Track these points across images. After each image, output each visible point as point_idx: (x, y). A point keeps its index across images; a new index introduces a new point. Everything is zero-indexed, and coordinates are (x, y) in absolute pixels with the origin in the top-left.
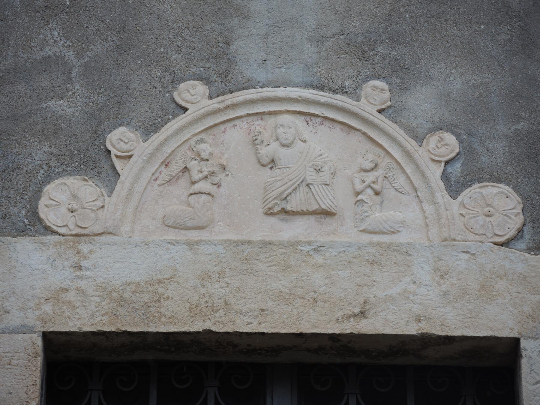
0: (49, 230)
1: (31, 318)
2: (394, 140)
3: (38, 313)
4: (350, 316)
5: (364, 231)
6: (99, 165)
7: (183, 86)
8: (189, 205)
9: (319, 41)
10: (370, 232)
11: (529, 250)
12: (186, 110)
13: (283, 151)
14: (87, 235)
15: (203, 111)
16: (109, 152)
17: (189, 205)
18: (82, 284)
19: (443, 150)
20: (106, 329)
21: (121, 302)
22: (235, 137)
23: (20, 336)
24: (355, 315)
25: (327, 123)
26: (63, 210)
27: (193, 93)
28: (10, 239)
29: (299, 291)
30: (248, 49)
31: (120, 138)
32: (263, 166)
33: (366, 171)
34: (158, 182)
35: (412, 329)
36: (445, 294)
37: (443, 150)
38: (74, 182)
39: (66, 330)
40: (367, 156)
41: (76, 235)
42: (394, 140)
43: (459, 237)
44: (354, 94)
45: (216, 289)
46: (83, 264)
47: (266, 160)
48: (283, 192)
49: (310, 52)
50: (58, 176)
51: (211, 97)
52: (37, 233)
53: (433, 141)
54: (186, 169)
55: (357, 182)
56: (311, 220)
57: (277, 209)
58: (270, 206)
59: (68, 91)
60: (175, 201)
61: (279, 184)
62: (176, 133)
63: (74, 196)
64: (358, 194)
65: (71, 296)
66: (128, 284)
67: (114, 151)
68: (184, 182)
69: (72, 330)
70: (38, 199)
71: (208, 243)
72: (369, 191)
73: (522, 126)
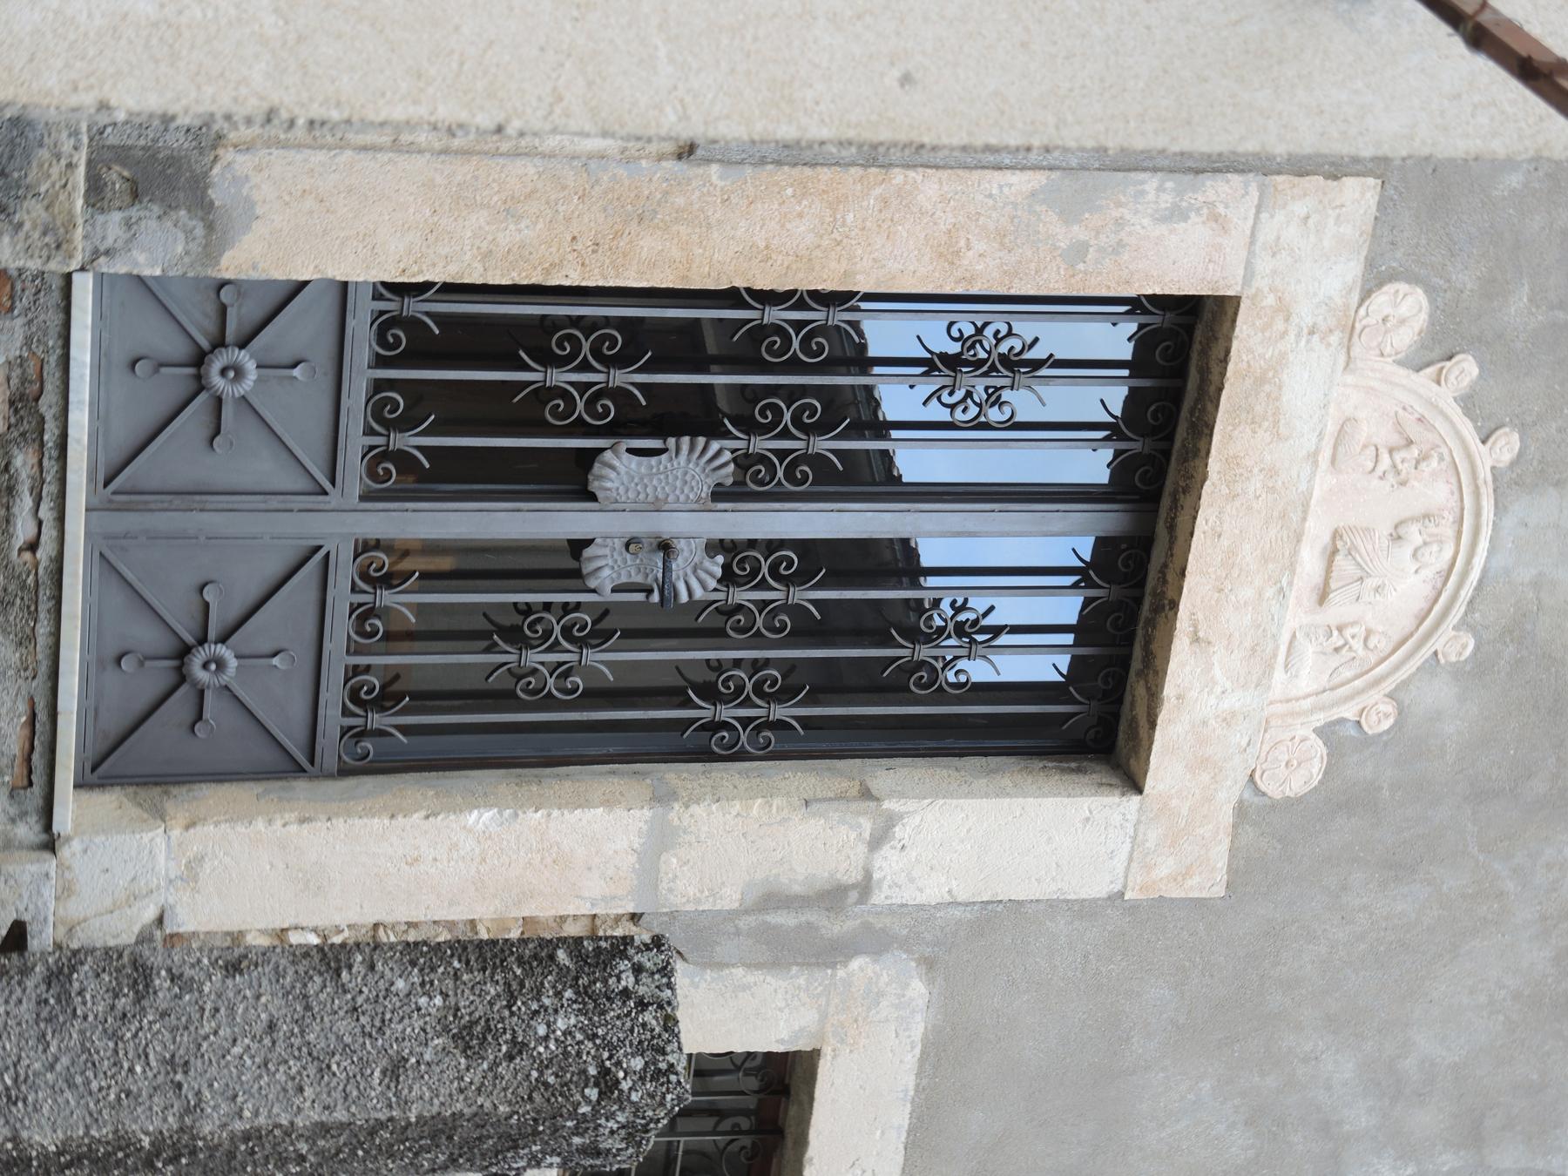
0: (1366, 295)
1: (1260, 283)
2: (1397, 668)
3: (1266, 290)
4: (1195, 627)
5: (1294, 636)
6: (1434, 351)
7: (1516, 436)
8: (1365, 447)
9: (1536, 584)
10: (1291, 643)
11: (1241, 802)
12: (1484, 442)
13: (1409, 550)
14: (1350, 339)
15: (1479, 462)
16: (1450, 358)
17: (1365, 447)
18: (1292, 337)
19: (1374, 718)
20: (1231, 367)
21: (1261, 381)
22: (1435, 492)
23: (1241, 272)
24: (1196, 632)
25: (1432, 594)
26: (1387, 311)
28: (1364, 253)
29: (1235, 573)
31: (1466, 369)
32: (1396, 527)
33: (1366, 640)
34: (1401, 412)
35: (1169, 690)
36: (1205, 723)
37: (1374, 718)
39: (1239, 323)
41: (1353, 327)
42: (1397, 668)
43: (1267, 736)
44: (1464, 624)
45: (1255, 484)
46: (1316, 338)
47: (1402, 531)
48: (1358, 551)
49: (1526, 575)
50: (1432, 301)
51: (1493, 468)
52: (1365, 281)
53: (1389, 708)
54: (1410, 443)
55: (1355, 630)
56: (1317, 578)
57: (1339, 544)
58: (1345, 537)
59: (1538, 307)
60: (1374, 429)
61: (1370, 547)
62: (1458, 434)
63: (1402, 322)
64: (1340, 629)
65: (1279, 325)
66: (1280, 388)
67: (1448, 364)
68: (1395, 439)
69: (1237, 330)
70: (1409, 281)
71: (1314, 473)
72: (1341, 643)
73: (1386, 793)
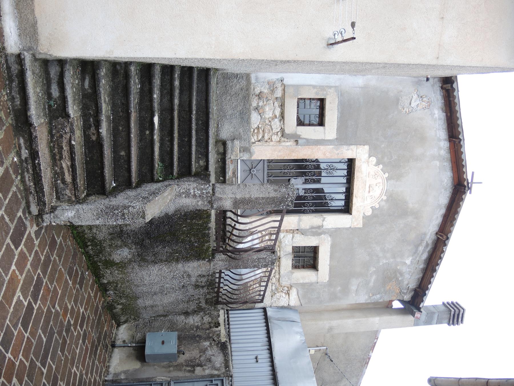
6: (377, 164)
27: (387, 175)
30: (392, 182)
38: (375, 161)
40: (376, 197)
45: (360, 179)
